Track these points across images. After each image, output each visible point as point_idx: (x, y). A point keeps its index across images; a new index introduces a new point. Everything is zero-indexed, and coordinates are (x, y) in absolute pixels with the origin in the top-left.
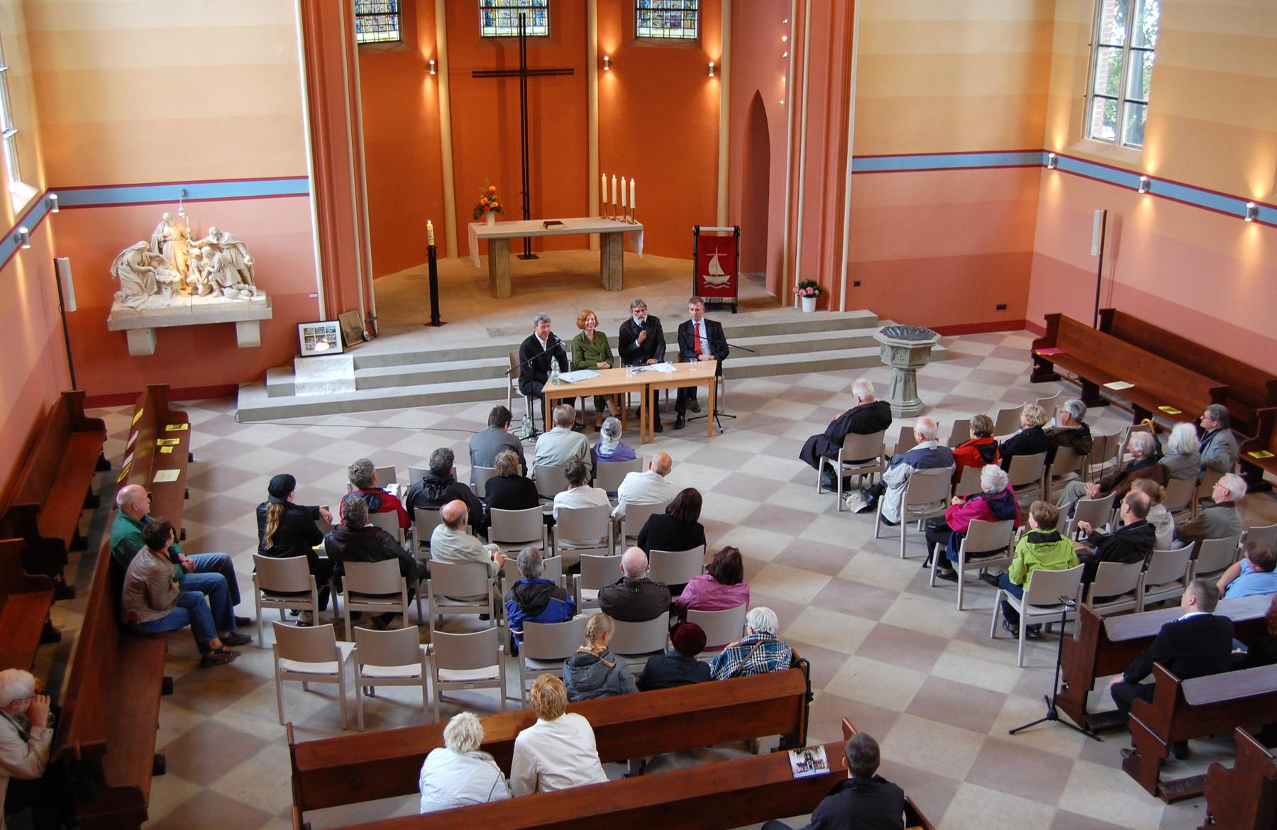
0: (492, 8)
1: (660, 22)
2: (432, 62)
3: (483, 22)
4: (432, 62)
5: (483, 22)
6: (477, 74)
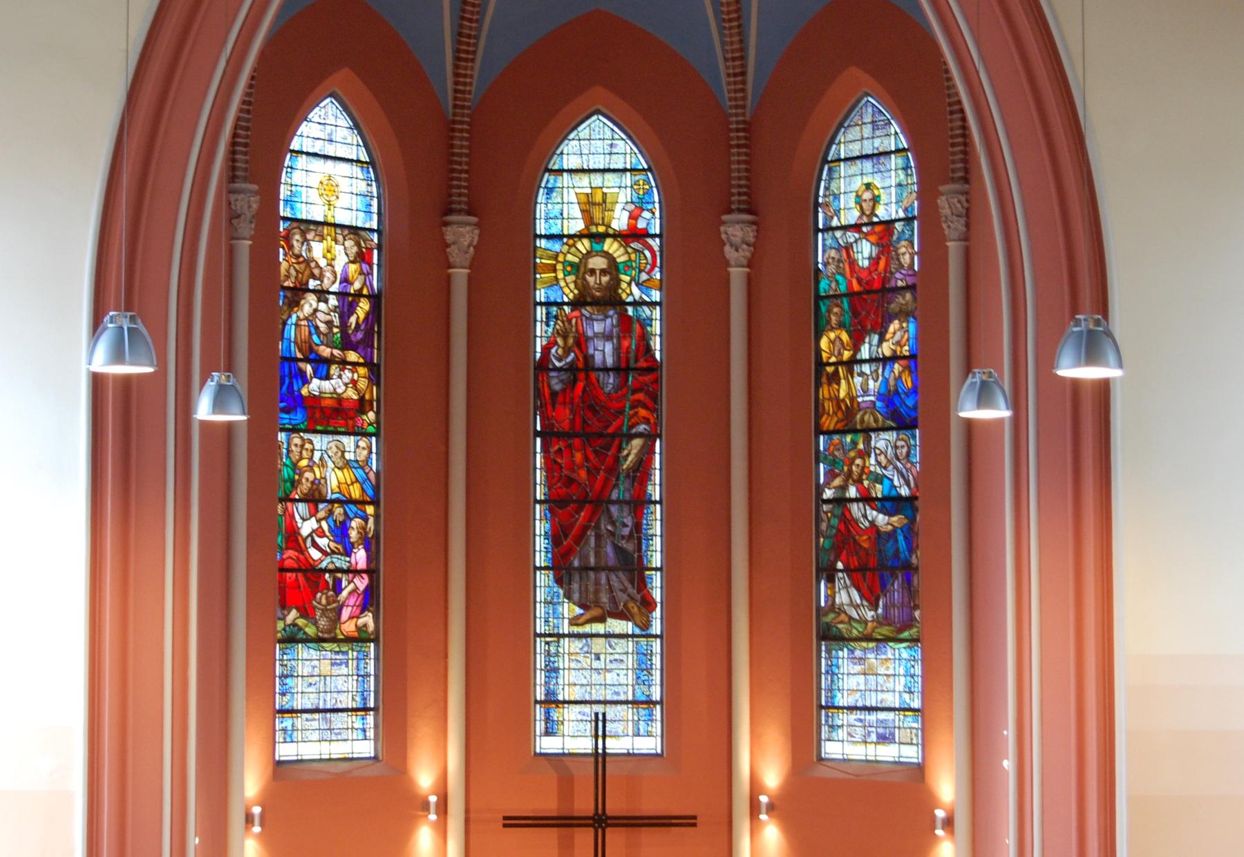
0: (558, 703)
1: (859, 732)
2: (433, 799)
3: (540, 727)
4: (433, 799)
5: (540, 727)
6: (512, 822)
